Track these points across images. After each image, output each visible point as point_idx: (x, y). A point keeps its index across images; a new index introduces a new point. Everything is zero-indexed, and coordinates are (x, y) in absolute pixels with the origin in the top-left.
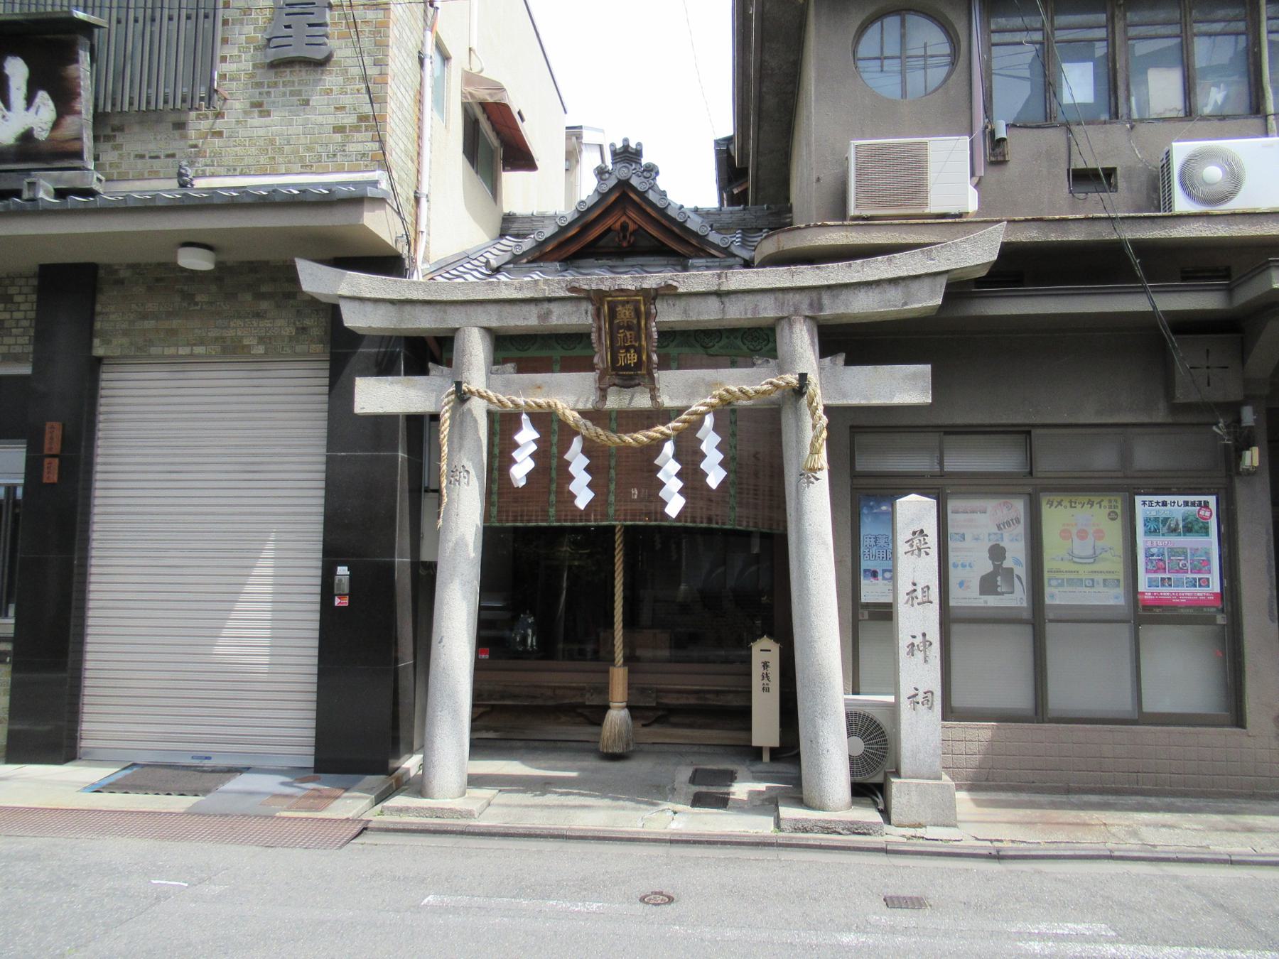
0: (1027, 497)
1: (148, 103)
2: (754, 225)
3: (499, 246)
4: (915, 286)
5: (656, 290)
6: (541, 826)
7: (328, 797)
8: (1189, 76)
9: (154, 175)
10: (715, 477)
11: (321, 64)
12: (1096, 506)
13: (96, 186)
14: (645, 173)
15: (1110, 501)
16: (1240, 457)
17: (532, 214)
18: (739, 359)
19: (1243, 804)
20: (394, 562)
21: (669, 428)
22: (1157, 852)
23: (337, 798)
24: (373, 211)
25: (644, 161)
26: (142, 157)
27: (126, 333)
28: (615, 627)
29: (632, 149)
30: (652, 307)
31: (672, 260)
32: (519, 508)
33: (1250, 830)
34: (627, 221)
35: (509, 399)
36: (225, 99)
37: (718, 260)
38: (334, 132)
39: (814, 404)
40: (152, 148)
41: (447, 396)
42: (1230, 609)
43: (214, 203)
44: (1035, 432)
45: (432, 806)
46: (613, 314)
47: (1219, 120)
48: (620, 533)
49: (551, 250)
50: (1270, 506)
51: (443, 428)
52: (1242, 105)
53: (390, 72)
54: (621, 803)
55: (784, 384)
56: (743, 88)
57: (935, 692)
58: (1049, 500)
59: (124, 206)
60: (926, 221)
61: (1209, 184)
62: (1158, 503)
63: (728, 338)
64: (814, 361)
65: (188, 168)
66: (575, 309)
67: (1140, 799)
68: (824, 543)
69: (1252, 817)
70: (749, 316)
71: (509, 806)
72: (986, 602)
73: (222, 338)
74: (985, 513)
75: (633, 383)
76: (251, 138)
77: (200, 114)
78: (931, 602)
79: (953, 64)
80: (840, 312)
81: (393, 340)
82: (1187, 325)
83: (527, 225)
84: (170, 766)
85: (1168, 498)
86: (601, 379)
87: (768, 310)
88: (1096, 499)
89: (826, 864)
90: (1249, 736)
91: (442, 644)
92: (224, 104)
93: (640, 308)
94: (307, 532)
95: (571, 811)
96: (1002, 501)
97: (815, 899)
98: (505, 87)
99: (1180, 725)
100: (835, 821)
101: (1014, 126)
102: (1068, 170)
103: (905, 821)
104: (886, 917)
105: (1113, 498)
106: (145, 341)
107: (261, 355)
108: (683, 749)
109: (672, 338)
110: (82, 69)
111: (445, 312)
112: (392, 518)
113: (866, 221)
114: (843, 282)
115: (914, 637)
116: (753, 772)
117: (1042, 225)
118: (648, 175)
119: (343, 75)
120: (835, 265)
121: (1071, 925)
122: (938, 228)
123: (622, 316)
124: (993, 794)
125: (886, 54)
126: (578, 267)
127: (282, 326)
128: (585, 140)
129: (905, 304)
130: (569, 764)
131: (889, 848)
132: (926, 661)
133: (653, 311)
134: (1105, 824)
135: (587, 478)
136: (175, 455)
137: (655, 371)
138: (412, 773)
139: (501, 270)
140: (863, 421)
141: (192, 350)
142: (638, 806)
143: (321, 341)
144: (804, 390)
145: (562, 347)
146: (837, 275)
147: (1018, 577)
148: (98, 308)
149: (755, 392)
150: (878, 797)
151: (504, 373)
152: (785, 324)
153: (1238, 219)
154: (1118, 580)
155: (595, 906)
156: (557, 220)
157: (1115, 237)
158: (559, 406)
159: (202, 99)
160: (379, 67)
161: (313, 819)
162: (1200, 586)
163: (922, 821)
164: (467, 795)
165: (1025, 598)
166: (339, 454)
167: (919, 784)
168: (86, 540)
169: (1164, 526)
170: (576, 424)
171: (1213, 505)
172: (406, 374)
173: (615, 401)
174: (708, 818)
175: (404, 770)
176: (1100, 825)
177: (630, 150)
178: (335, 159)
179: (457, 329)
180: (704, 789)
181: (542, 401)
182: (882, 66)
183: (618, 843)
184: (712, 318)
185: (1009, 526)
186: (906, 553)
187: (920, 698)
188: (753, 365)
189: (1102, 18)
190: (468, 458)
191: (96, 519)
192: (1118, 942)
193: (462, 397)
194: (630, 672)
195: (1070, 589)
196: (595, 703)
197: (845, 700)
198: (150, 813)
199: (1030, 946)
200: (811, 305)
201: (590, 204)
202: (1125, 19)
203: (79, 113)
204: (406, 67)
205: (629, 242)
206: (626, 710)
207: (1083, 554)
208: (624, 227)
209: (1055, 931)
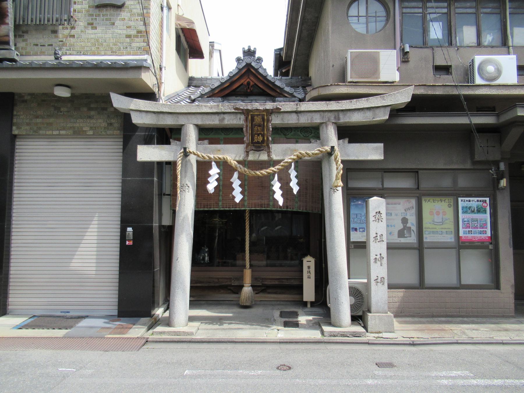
0: (417, 198)
1: (40, 21)
2: (296, 85)
3: (188, 90)
4: (377, 111)
5: (272, 110)
6: (224, 338)
7: (126, 328)
8: (479, 30)
9: (42, 53)
10: (296, 189)
11: (120, 7)
12: (443, 202)
13: (16, 58)
14: (257, 61)
15: (449, 200)
16: (499, 183)
17: (202, 77)
18: (300, 140)
19: (499, 320)
20: (152, 226)
21: (275, 169)
22: (474, 340)
23: (131, 328)
24: (145, 73)
25: (257, 55)
26: (37, 45)
27: (28, 124)
28: (246, 252)
29: (252, 50)
30: (270, 117)
31: (268, 98)
32: (206, 202)
33: (506, 330)
34: (250, 81)
35: (206, 155)
36: (76, 21)
37: (288, 98)
38: (126, 38)
39: (337, 159)
40: (41, 41)
41: (180, 154)
42: (494, 243)
43: (71, 67)
44: (420, 172)
45: (175, 330)
46: (253, 120)
47: (491, 48)
48: (248, 213)
49: (218, 92)
50: (509, 202)
51: (178, 168)
52: (498, 42)
53: (151, 12)
54: (254, 327)
55: (324, 151)
56: (290, 28)
57: (385, 278)
58: (425, 200)
59: (31, 67)
60: (379, 84)
61: (490, 73)
62: (467, 200)
63: (295, 131)
64: (336, 141)
65: (59, 51)
66: (235, 117)
67: (461, 319)
68: (340, 217)
69: (505, 325)
70: (309, 122)
71: (207, 329)
72: (400, 241)
73: (74, 127)
74: (400, 204)
75: (260, 149)
76: (88, 39)
77: (64, 27)
78: (383, 241)
79: (387, 20)
80: (347, 121)
81: (152, 129)
82: (482, 129)
83: (200, 82)
84: (50, 316)
85: (471, 199)
86: (247, 147)
87: (317, 119)
88: (443, 199)
89: (347, 350)
90: (502, 293)
91: (178, 261)
92: (75, 23)
93: (264, 117)
94: (112, 213)
95: (235, 331)
96: (406, 200)
97: (349, 365)
98: (195, 22)
99: (471, 289)
100: (346, 332)
101: (412, 47)
102: (433, 66)
103: (374, 331)
104: (380, 372)
105: (450, 199)
106: (37, 128)
107: (91, 135)
108: (273, 303)
109: (231, 131)
110: (9, 4)
111: (178, 117)
112: (152, 207)
113: (355, 84)
114: (348, 108)
115: (376, 255)
116: (304, 312)
117: (426, 87)
118: (259, 62)
119: (130, 12)
120: (345, 101)
121: (455, 372)
122: (384, 87)
123: (257, 121)
124: (404, 318)
125: (360, 15)
126: (228, 100)
127: (101, 122)
128: (215, 48)
129: (374, 118)
130: (227, 310)
131: (370, 342)
132: (381, 265)
133: (270, 119)
134: (451, 330)
135: (240, 189)
136: (55, 179)
137: (270, 144)
138: (160, 316)
139: (196, 100)
140: (352, 167)
141: (59, 132)
142: (262, 328)
143: (119, 130)
144: (332, 153)
145: (204, 134)
146: (346, 106)
147: (413, 230)
148: (15, 113)
149: (312, 154)
150: (360, 321)
151: (204, 144)
152: (324, 125)
153: (501, 87)
154: (452, 232)
155: (259, 372)
156: (220, 80)
157: (458, 93)
158: (228, 158)
159: (65, 20)
160: (146, 10)
161: (123, 338)
162: (483, 234)
163: (381, 330)
164: (188, 325)
165: (415, 239)
166: (128, 179)
167: (379, 316)
168: (10, 216)
169: (469, 210)
170: (236, 167)
171: (488, 202)
172: (157, 144)
173: (252, 157)
174: (292, 332)
175: (157, 315)
176: (449, 330)
177: (251, 51)
178: (127, 50)
179: (183, 125)
180: (287, 320)
181: (221, 156)
182: (358, 20)
183: (258, 344)
184: (293, 122)
185: (409, 210)
186: (373, 221)
187: (379, 280)
188: (310, 142)
189: (446, 4)
190: (189, 181)
191: (14, 207)
192: (476, 378)
193: (186, 154)
194: (252, 271)
195: (433, 235)
196: (236, 284)
197: (349, 281)
198: (47, 338)
199: (443, 381)
200: (335, 118)
201: (234, 73)
202: (455, 5)
203: (8, 24)
204: (157, 11)
205: (250, 90)
206: (251, 287)
207: (438, 221)
208: (248, 84)
209: (449, 375)
